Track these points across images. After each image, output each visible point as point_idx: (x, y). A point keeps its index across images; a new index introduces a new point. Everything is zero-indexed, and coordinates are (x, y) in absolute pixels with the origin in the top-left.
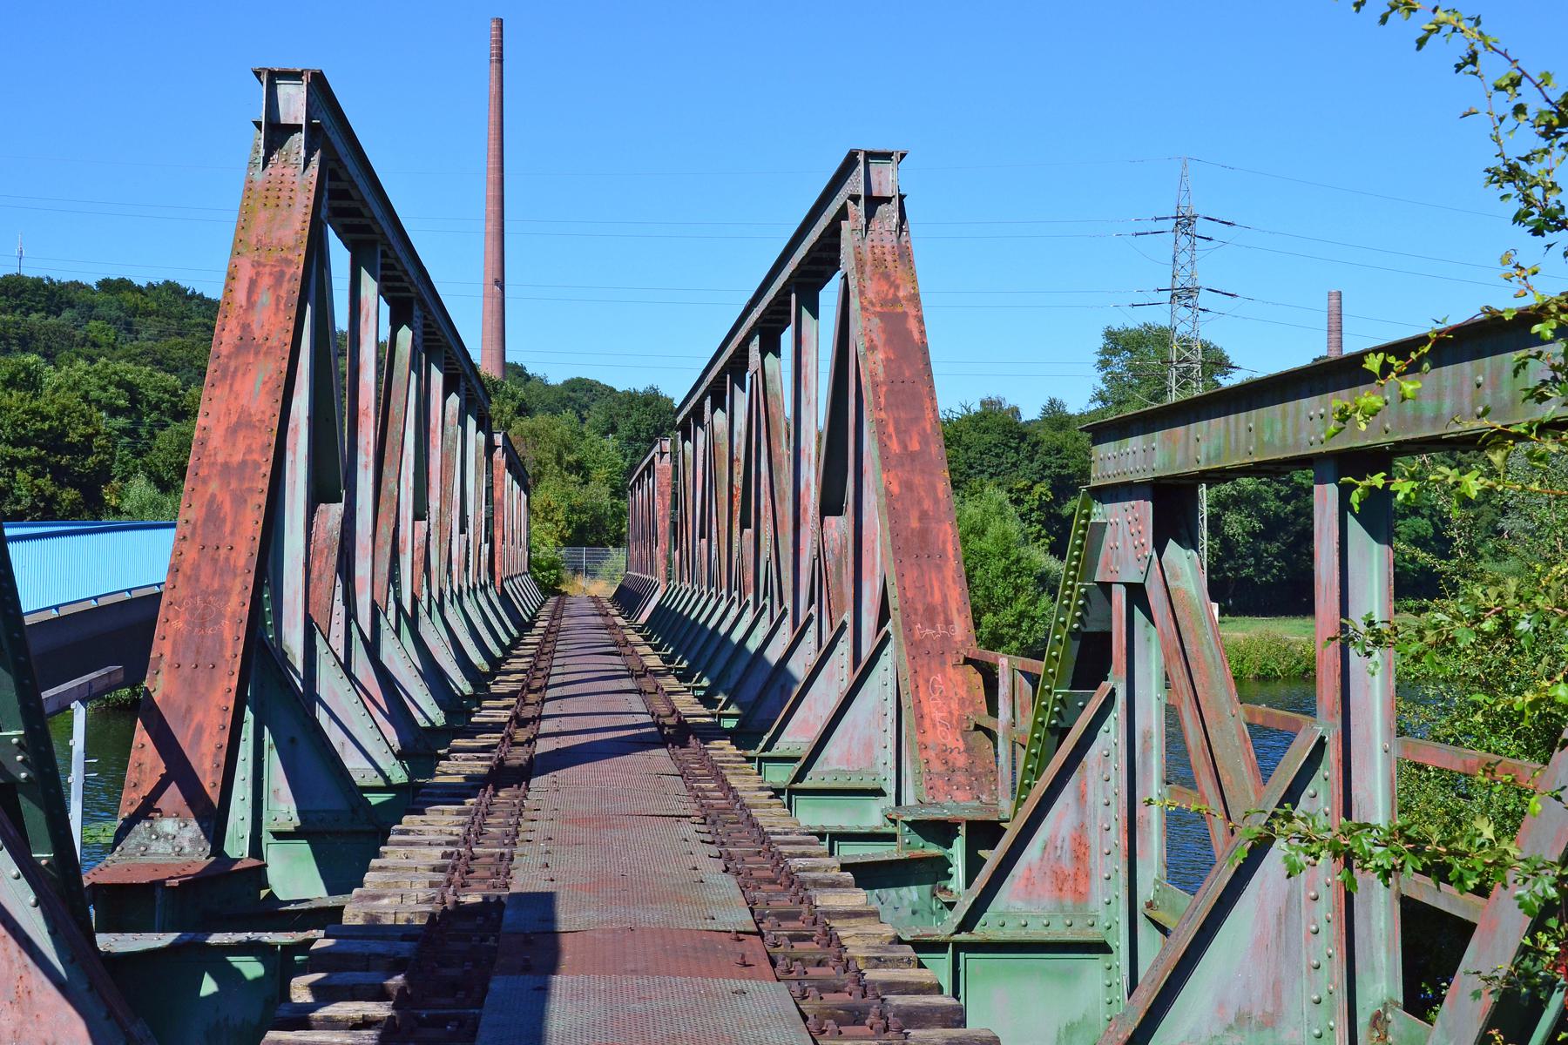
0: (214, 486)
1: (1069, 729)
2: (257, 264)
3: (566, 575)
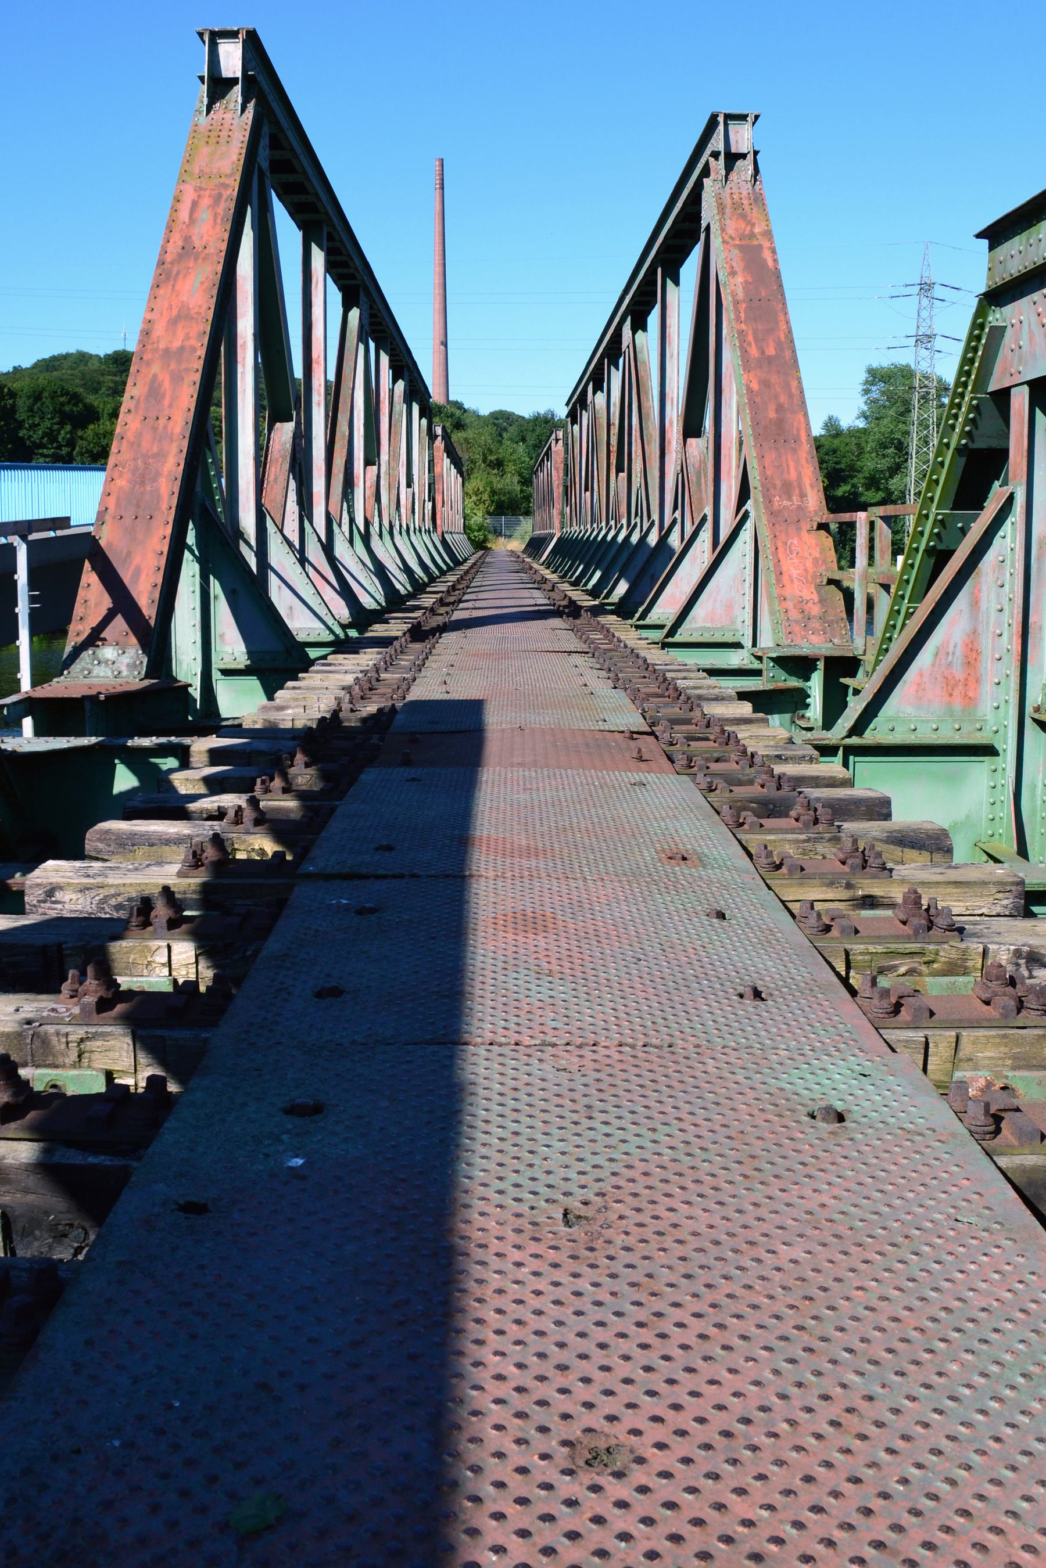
0: (156, 368)
1: (952, 552)
2: (198, 189)
3: (490, 537)
